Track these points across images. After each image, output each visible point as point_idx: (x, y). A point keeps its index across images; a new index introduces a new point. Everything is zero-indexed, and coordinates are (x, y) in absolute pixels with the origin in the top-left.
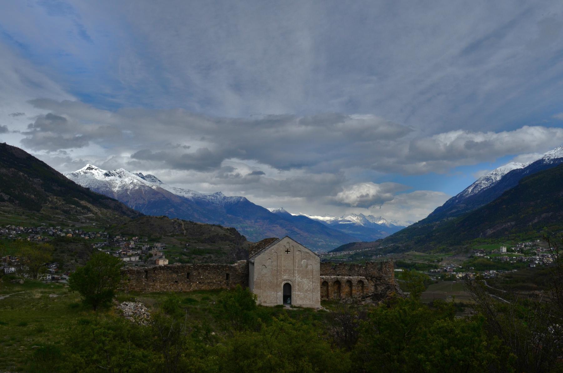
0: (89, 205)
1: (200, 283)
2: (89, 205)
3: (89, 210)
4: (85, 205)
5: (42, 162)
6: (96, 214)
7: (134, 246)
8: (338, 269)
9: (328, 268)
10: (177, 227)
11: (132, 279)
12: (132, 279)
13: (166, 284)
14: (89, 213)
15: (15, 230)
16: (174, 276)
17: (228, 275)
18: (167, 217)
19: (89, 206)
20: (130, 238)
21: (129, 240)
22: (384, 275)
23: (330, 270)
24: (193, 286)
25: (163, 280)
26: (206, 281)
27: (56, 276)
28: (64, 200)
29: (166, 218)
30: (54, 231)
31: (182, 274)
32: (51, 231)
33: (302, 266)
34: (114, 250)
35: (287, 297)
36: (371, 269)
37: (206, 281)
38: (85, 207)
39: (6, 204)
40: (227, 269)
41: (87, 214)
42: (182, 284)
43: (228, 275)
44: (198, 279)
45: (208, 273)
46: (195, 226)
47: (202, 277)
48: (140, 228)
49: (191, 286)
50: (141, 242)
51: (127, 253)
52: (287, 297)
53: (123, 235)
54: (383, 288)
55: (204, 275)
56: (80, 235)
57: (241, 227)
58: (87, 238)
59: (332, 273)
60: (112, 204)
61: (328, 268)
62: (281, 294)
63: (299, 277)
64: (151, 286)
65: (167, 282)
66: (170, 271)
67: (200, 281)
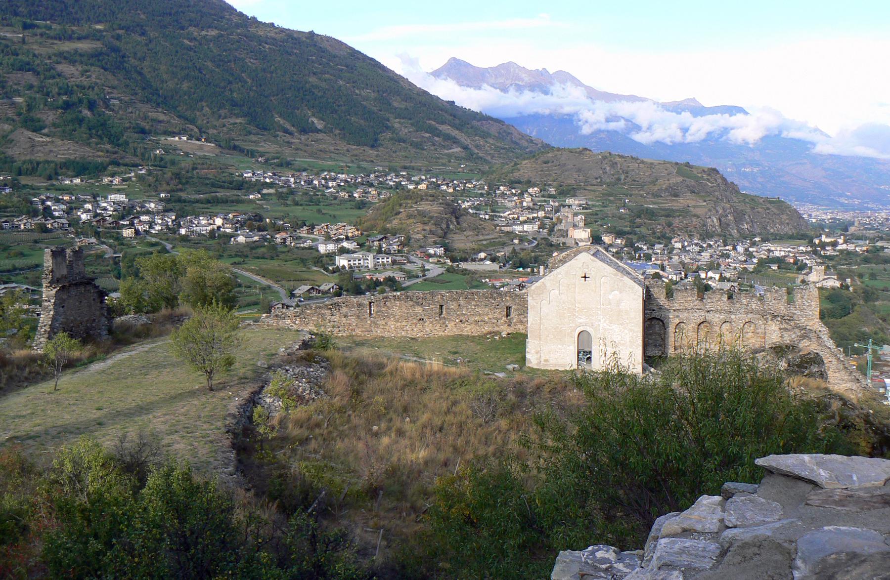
0: (455, 133)
1: (461, 321)
2: (455, 133)
3: (455, 141)
4: (448, 132)
5: (372, 59)
6: (465, 148)
7: (531, 205)
8: (709, 300)
9: (689, 299)
10: (608, 168)
11: (351, 316)
12: (351, 316)
13: (404, 323)
14: (454, 146)
15: (334, 180)
16: (418, 309)
17: (508, 308)
18: (590, 150)
19: (453, 134)
20: (524, 190)
21: (522, 194)
22: (798, 312)
23: (693, 302)
24: (449, 326)
25: (401, 316)
26: (472, 319)
27: (398, 258)
28: (412, 124)
29: (588, 152)
30: (397, 180)
31: (431, 306)
32: (391, 180)
33: (610, 304)
34: (498, 212)
35: (585, 355)
36: (774, 302)
37: (472, 319)
38: (447, 137)
39: (320, 136)
40: (508, 298)
41: (451, 149)
42: (431, 322)
43: (508, 308)
44: (458, 315)
45: (475, 306)
46: (641, 165)
47: (464, 312)
48: (542, 171)
49: (447, 326)
50: (543, 196)
51: (518, 217)
52: (585, 355)
53: (512, 184)
54: (793, 336)
55: (468, 309)
56: (439, 186)
57: (734, 164)
58: (451, 190)
59: (698, 307)
60: (494, 130)
61: (689, 299)
62: (573, 349)
63: (605, 321)
64: (381, 327)
65: (407, 319)
66: (411, 303)
67: (462, 318)
